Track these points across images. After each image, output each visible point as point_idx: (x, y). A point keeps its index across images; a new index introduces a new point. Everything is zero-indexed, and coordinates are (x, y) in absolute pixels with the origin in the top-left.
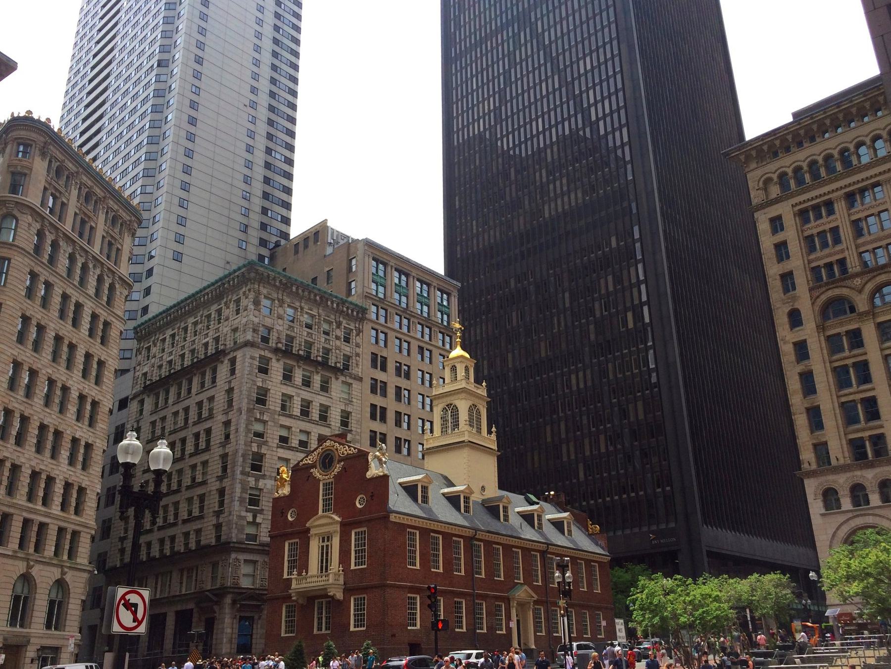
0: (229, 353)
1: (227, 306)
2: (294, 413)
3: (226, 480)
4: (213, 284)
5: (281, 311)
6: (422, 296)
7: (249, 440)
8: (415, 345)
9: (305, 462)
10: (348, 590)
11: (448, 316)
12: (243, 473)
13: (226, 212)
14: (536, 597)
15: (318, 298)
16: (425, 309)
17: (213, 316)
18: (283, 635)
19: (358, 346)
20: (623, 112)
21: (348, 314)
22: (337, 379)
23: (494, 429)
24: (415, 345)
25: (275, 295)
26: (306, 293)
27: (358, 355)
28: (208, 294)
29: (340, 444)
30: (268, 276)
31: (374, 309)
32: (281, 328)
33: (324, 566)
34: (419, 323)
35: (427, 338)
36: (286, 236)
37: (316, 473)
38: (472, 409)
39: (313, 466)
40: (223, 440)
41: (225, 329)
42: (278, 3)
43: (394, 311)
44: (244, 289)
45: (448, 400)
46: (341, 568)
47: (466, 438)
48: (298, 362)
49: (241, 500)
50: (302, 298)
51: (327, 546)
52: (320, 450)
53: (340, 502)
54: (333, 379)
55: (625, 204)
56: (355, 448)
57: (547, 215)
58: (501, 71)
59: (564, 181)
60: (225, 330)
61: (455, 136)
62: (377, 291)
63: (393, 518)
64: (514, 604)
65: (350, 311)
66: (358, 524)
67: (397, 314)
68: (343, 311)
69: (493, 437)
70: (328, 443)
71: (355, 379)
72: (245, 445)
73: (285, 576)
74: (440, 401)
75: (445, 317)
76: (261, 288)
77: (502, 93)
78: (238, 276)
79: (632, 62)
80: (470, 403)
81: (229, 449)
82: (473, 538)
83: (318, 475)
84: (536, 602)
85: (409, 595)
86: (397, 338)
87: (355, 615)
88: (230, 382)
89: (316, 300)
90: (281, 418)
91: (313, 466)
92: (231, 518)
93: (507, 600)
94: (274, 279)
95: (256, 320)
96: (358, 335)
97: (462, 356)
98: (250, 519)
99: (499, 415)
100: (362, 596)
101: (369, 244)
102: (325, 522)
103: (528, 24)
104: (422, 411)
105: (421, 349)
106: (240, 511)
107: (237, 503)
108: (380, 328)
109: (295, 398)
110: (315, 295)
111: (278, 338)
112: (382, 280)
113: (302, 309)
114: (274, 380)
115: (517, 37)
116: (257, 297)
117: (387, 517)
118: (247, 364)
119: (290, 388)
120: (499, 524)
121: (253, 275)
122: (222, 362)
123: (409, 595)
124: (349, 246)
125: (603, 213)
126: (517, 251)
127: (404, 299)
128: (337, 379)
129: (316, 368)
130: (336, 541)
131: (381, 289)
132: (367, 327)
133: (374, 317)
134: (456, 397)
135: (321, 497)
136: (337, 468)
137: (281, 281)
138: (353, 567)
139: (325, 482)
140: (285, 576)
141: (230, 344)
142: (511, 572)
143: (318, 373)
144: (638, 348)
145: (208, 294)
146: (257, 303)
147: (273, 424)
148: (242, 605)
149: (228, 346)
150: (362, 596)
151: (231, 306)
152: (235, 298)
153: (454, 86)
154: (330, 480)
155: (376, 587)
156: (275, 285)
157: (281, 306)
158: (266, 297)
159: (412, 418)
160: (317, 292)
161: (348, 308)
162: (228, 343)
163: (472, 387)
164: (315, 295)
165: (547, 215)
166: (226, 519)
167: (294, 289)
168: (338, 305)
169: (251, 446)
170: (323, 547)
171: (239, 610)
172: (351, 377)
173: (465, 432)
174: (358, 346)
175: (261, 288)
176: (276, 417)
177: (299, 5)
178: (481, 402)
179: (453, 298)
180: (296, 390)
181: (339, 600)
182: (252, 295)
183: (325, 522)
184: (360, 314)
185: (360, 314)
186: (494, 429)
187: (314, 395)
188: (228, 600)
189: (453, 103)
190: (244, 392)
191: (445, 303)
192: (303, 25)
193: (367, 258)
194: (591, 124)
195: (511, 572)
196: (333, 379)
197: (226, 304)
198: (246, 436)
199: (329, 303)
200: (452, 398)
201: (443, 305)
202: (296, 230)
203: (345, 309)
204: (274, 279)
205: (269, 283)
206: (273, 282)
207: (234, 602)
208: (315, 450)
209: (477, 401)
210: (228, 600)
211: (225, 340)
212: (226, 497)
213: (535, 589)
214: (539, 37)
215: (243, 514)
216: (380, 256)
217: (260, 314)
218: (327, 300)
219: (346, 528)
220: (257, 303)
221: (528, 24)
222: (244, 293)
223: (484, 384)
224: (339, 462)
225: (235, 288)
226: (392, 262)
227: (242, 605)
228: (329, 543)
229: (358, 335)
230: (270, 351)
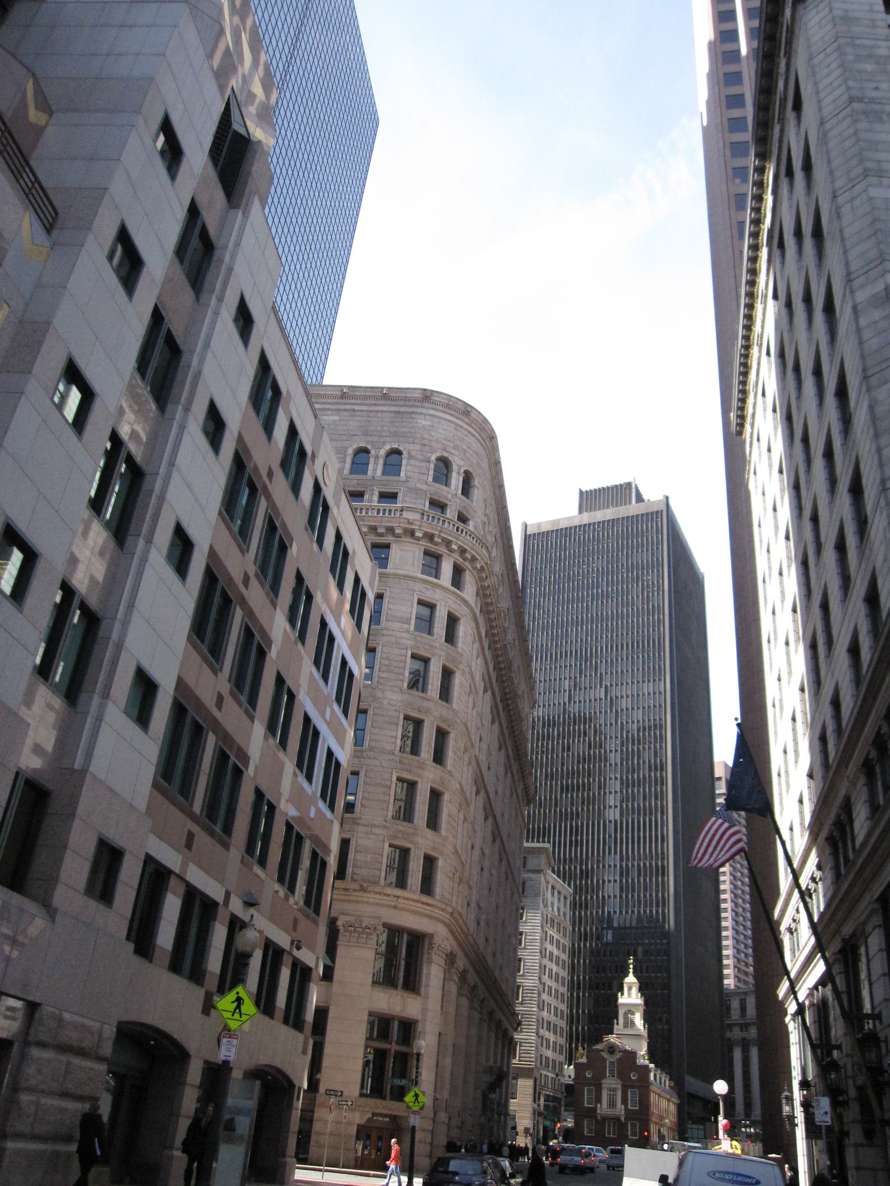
33: (612, 1104)
130: (619, 1094)
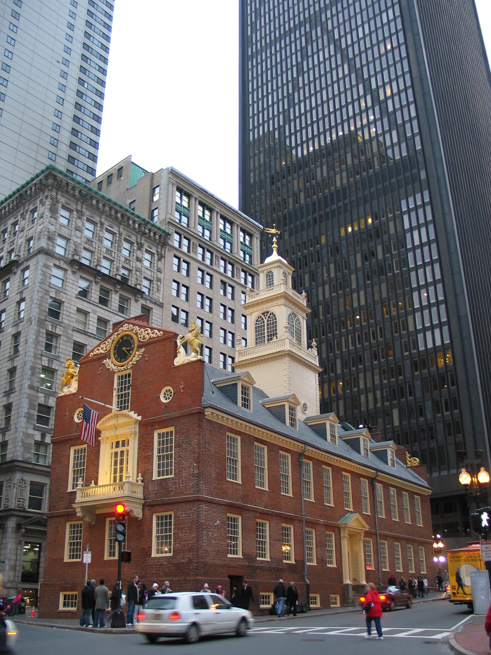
0: (22, 263)
1: (23, 217)
2: (90, 331)
3: (12, 395)
4: (10, 197)
5: (79, 223)
6: (225, 232)
7: (40, 352)
8: (217, 279)
9: (96, 352)
10: (149, 506)
11: (250, 257)
12: (31, 387)
13: (34, 155)
14: (367, 528)
15: (119, 215)
16: (228, 245)
17: (9, 230)
18: (66, 560)
19: (159, 271)
20: (410, 91)
21: (150, 237)
22: (137, 301)
23: (314, 343)
24: (217, 279)
25: (73, 206)
26: (107, 208)
27: (159, 280)
28: (5, 207)
29: (140, 327)
30: (67, 184)
31: (177, 237)
32: (78, 241)
34: (222, 259)
35: (229, 274)
36: (92, 171)
37: (110, 363)
38: (292, 316)
39: (106, 356)
40: (12, 353)
41: (20, 240)
42: (91, 2)
43: (197, 242)
44: (41, 198)
45: (264, 308)
46: (140, 478)
47: (287, 347)
48: (95, 277)
49: (29, 417)
50: (102, 213)
51: (122, 452)
52: (115, 336)
53: (139, 397)
54: (133, 301)
55: (415, 171)
56: (159, 330)
57: (338, 184)
58: (285, 94)
59: (344, 174)
60: (20, 241)
61: (251, 120)
62: (180, 220)
63: (208, 412)
64: (344, 534)
65: (152, 234)
66: (163, 424)
67: (200, 246)
68: (146, 234)
69: (315, 351)
70: (125, 327)
71: (155, 303)
72: (35, 357)
73: (70, 489)
74: (256, 309)
75: (247, 257)
76: (59, 197)
77: (286, 113)
78: (36, 184)
79: (418, 50)
80: (290, 311)
81: (18, 362)
82: (301, 455)
83: (112, 367)
84: (367, 534)
85: (229, 515)
86: (199, 269)
87: (158, 537)
88: (21, 292)
89: (116, 218)
90: (75, 333)
91: (106, 356)
92: (17, 435)
93: (337, 529)
94: (74, 188)
95: (52, 228)
96: (159, 260)
97: (280, 261)
98: (38, 438)
99: (319, 331)
100: (168, 513)
101: (173, 173)
102: (119, 426)
103: (319, 23)
104: (224, 346)
105: (224, 283)
106: (27, 428)
107: (24, 420)
108: (183, 257)
109: (91, 315)
110: (117, 212)
111: (75, 250)
112: (186, 211)
113: (102, 224)
114: (69, 293)
115: (308, 35)
116: (54, 205)
117: (201, 413)
118: (39, 272)
119: (86, 304)
120: (326, 443)
121: (50, 181)
122: (15, 273)
123: (229, 515)
124: (152, 180)
125: (394, 180)
126: (310, 218)
127: (207, 233)
128: (137, 301)
129: (115, 287)
131: (184, 219)
132: (169, 255)
133: (176, 245)
134: (274, 303)
135: (115, 393)
136: (136, 356)
137: (80, 192)
138: (155, 477)
139: (120, 374)
140: (70, 489)
141: (23, 254)
142: (340, 496)
143: (116, 292)
144: (350, 370)
145: (5, 207)
146: (54, 211)
147: (65, 339)
148: (27, 530)
149: (22, 257)
150: (168, 513)
151: (27, 216)
152: (31, 207)
153: (250, 78)
154: (127, 372)
155: (187, 501)
156: (74, 196)
157: (79, 218)
158: (64, 207)
159: (213, 351)
160: (119, 209)
161: (150, 230)
162: (21, 254)
163: (291, 292)
164: (117, 212)
165: (338, 184)
166: (12, 437)
167: (94, 202)
168: (140, 225)
169: (41, 360)
170: (116, 453)
171: (24, 536)
172: (151, 302)
173: (284, 341)
174: (159, 271)
175: (59, 197)
176: (70, 332)
177: (111, 7)
178: (301, 313)
179: (255, 240)
180: (93, 307)
181: (136, 519)
182: (48, 202)
183: (119, 426)
184: (162, 240)
185: (162, 240)
186: (314, 343)
187: (112, 315)
188: (11, 524)
189: (249, 93)
190: (35, 301)
191: (247, 243)
192: (114, 25)
193: (171, 186)
194: (380, 103)
195: (340, 496)
196: (133, 301)
197: (22, 215)
198: (36, 348)
199: (131, 222)
200: (269, 305)
201: (245, 245)
202: (102, 168)
203: (147, 231)
204: (74, 188)
205: (67, 192)
206: (72, 192)
207: (19, 526)
208: (112, 335)
209: (296, 310)
210: (11, 524)
211: (19, 251)
212: (13, 413)
213: (365, 517)
214: (330, 34)
215: (31, 431)
216: (185, 187)
217: (55, 225)
218: (129, 218)
219: (146, 429)
220: (54, 211)
221: (319, 23)
222: (41, 201)
223: (304, 293)
224: (139, 347)
225: (32, 198)
226: (196, 194)
227: (27, 530)
228: (124, 449)
229: (159, 260)
230: (66, 262)
